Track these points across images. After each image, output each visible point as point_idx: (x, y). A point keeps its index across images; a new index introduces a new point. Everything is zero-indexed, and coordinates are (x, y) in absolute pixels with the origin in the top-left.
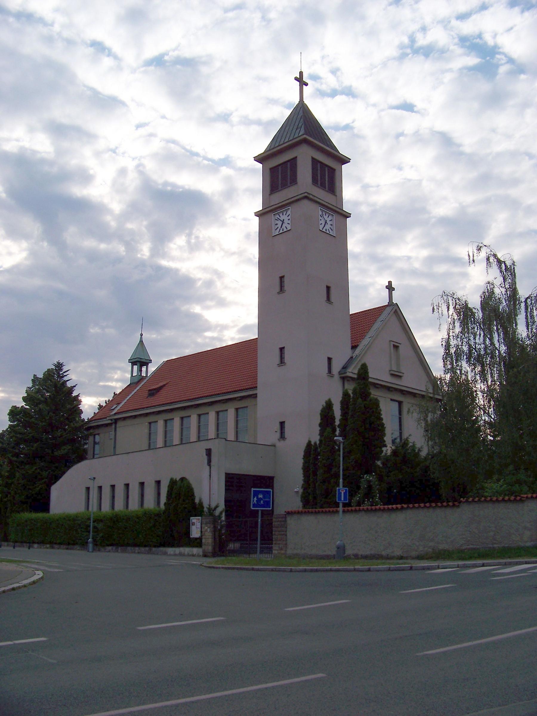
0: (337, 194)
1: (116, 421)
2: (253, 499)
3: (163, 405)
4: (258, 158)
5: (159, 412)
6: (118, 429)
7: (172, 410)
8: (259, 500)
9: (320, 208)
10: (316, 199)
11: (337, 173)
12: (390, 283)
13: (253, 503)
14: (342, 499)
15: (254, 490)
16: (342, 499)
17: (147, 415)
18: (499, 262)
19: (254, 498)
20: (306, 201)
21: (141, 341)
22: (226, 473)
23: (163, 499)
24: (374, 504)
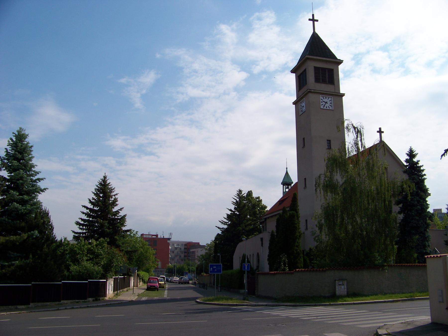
1: (266, 219)
2: (210, 268)
8: (214, 269)
12: (380, 129)
14: (246, 269)
16: (246, 269)
18: (355, 128)
19: (210, 268)
20: (310, 95)
21: (287, 173)
24: (413, 262)
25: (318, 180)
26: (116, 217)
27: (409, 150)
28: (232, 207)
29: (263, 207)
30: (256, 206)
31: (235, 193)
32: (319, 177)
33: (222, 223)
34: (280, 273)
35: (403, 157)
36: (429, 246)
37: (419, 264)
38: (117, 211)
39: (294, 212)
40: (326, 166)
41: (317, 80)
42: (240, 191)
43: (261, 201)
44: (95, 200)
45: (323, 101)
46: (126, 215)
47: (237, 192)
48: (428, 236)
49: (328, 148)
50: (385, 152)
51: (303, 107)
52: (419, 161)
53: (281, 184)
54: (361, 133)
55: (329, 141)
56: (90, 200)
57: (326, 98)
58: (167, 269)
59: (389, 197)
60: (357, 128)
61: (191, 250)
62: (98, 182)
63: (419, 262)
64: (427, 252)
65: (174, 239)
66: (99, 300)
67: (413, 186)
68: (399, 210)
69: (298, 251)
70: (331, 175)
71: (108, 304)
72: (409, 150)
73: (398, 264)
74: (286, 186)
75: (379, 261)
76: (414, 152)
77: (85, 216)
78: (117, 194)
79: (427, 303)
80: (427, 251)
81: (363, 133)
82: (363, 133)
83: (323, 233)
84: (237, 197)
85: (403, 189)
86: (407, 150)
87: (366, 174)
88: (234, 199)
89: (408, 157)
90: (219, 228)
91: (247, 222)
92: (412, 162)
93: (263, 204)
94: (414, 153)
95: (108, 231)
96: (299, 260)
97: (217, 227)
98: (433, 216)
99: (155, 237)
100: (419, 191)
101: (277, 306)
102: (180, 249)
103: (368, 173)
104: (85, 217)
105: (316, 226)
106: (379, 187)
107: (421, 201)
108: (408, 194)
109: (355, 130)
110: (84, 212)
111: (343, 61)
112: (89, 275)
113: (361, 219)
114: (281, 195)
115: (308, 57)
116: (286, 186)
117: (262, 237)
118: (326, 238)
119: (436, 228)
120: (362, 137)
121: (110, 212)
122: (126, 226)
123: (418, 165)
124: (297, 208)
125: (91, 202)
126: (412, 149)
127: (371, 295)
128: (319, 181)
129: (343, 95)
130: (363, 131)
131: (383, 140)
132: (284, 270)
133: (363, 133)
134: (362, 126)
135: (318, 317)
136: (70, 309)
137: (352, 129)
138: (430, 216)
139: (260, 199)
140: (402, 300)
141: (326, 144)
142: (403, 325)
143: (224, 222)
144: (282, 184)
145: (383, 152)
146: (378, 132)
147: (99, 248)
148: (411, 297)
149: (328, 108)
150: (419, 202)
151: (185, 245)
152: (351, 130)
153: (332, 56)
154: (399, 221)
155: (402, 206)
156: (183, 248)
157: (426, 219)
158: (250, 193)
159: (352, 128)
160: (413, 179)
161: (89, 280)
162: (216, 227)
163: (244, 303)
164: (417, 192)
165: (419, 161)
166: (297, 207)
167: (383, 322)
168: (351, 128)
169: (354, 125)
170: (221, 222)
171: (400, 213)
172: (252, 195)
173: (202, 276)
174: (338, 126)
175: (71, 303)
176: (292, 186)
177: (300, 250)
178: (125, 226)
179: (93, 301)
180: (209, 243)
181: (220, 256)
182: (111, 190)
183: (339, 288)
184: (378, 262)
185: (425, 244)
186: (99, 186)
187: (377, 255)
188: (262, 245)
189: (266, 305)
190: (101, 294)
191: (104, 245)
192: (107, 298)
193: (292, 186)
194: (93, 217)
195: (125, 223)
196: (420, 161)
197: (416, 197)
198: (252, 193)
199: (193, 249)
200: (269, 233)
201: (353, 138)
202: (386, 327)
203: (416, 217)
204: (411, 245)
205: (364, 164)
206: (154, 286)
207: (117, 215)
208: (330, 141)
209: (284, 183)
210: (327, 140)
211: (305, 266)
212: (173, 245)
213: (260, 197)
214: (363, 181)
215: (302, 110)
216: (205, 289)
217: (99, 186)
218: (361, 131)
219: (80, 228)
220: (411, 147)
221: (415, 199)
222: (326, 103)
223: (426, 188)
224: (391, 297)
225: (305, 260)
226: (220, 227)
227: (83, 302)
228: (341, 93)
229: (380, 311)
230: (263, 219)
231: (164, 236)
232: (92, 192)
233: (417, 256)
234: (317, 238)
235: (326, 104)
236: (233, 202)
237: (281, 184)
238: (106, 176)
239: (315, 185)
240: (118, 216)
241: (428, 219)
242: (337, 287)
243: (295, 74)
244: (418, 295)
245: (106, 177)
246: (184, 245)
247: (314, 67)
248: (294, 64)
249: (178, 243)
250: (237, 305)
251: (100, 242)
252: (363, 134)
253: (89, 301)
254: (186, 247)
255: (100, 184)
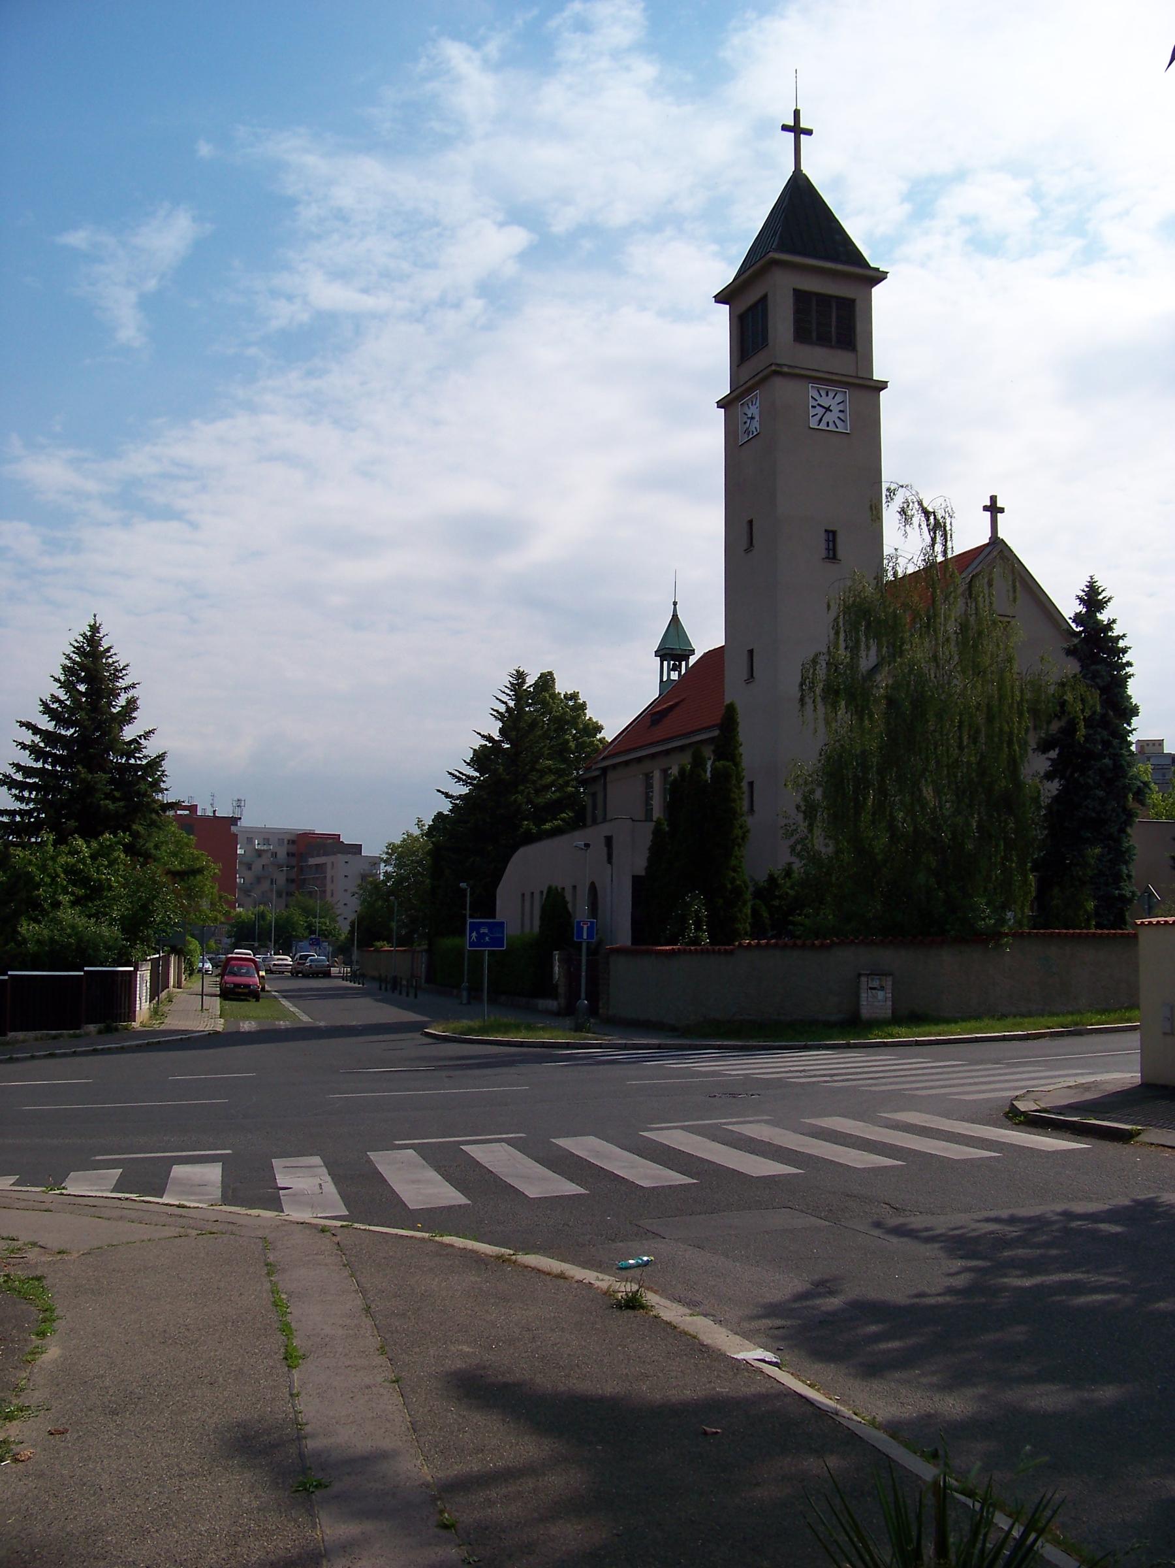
0: (859, 347)
1: (605, 770)
2: (470, 934)
3: (652, 744)
4: (718, 297)
5: (653, 756)
6: (609, 786)
7: (667, 753)
8: (481, 936)
9: (811, 385)
10: (797, 371)
11: (859, 306)
12: (993, 499)
13: (470, 939)
14: (585, 937)
15: (470, 922)
16: (585, 937)
17: (639, 760)
18: (927, 513)
20: (778, 382)
21: (675, 617)
22: (633, 876)
23: (537, 923)
24: (1083, 925)
25: (811, 671)
26: (130, 762)
27: (1087, 586)
28: (494, 729)
29: (591, 727)
30: (567, 724)
31: (505, 680)
32: (814, 662)
33: (458, 778)
34: (714, 951)
35: (1069, 607)
36: (1129, 876)
37: (1099, 931)
38: (134, 741)
39: (728, 764)
40: (833, 629)
41: (802, 335)
42: (520, 676)
43: (583, 707)
44: (61, 702)
45: (819, 405)
46: (165, 753)
47: (511, 679)
48: (1129, 847)
49: (827, 558)
50: (1015, 591)
51: (752, 418)
52: (1114, 621)
53: (656, 656)
54: (945, 529)
55: (831, 535)
56: (44, 704)
57: (827, 395)
58: (233, 926)
59: (1023, 733)
60: (934, 513)
61: (312, 861)
62: (71, 644)
63: (1098, 926)
64: (1124, 896)
65: (249, 820)
66: (117, 1029)
67: (1095, 699)
68: (1048, 769)
69: (738, 882)
70: (852, 659)
71: (153, 1042)
72: (1087, 586)
73: (1042, 931)
74: (672, 662)
75: (987, 920)
76: (1100, 594)
77: (30, 755)
78: (133, 686)
79: (1134, 1038)
80: (1124, 892)
81: (951, 530)
82: (949, 532)
83: (817, 832)
84: (510, 696)
85: (1063, 704)
86: (1079, 587)
87: (956, 658)
88: (500, 700)
89: (1081, 609)
90: (447, 795)
91: (541, 777)
92: (1095, 625)
93: (587, 718)
94: (1100, 597)
95: (111, 807)
96: (740, 911)
97: (443, 793)
98: (1147, 790)
99: (187, 812)
100: (1109, 711)
101: (691, 1048)
102: (275, 855)
103: (961, 653)
104: (26, 759)
105: (797, 809)
106: (995, 703)
107: (1116, 742)
108: (1078, 723)
109: (928, 520)
110: (25, 744)
111: (887, 273)
112: (82, 953)
113: (938, 792)
114: (650, 693)
115: (777, 256)
116: (672, 662)
117: (609, 834)
118: (827, 845)
119: (1148, 817)
120: (949, 543)
121: (114, 743)
122: (166, 790)
123: (1110, 634)
124: (737, 752)
125: (47, 710)
126: (1095, 582)
127: (964, 1020)
128: (814, 674)
129: (883, 385)
130: (951, 524)
131: (1001, 535)
132: (696, 941)
133: (949, 532)
134: (949, 509)
135: (836, 1078)
136: (45, 1056)
137: (918, 518)
138: (1139, 788)
139: (581, 701)
140: (1052, 1035)
141: (823, 545)
142: (1073, 1091)
143: (464, 777)
144: (657, 654)
145: (1008, 591)
146: (986, 508)
147: (103, 865)
148: (1077, 1024)
149: (832, 428)
150: (1107, 744)
151: (292, 842)
152: (915, 521)
153: (853, 256)
154: (1046, 800)
155: (1058, 755)
156: (282, 852)
157: (1126, 797)
158: (546, 681)
159: (920, 512)
160: (1095, 676)
161: (86, 969)
162: (439, 791)
163: (585, 1039)
164: (1104, 716)
165: (1114, 621)
166: (736, 748)
167: (1022, 1088)
168: (916, 513)
169: (925, 505)
170: (453, 775)
171: (1049, 776)
172: (553, 687)
173: (378, 951)
174: (874, 505)
175: (36, 1039)
176: (690, 666)
177: (744, 882)
178: (162, 791)
179: (100, 1032)
180: (398, 842)
181: (469, 890)
182: (116, 670)
183: (870, 999)
184: (986, 923)
185: (1120, 870)
186: (74, 656)
187: (981, 901)
188: (610, 859)
189: (659, 1047)
190: (123, 1011)
191: (116, 854)
192: (136, 1025)
193: (690, 666)
194: (57, 760)
195: (164, 782)
196: (1117, 622)
197: (1099, 729)
198: (553, 680)
199: (318, 855)
200: (633, 821)
201: (924, 545)
202: (1032, 1096)
203: (1097, 792)
204: (1080, 873)
205: (952, 627)
206: (247, 986)
207: (137, 755)
208: (834, 533)
209: (664, 653)
210: (826, 531)
211: (758, 931)
212: (250, 840)
213: (578, 693)
214: (945, 677)
215: (748, 429)
216: (400, 993)
217: (74, 656)
218: (945, 523)
219: (17, 798)
220: (1091, 577)
221: (1098, 737)
222: (828, 409)
223: (1131, 703)
224: (1019, 1026)
225: (755, 912)
226: (450, 793)
227: (71, 1036)
228: (874, 378)
229: (997, 1062)
230: (597, 769)
231: (215, 811)
232: (52, 676)
233: (1095, 906)
234: (799, 847)
235: (828, 413)
236: (495, 710)
237: (656, 656)
238: (98, 625)
239: (801, 685)
240: (140, 758)
241: (1130, 796)
242: (863, 995)
243: (727, 307)
244: (1093, 1021)
245: (98, 628)
246: (286, 842)
247: (794, 289)
248: (726, 274)
249: (267, 836)
250: (568, 1046)
251: (100, 844)
252: (951, 535)
253: (87, 1034)
254: (293, 849)
255: (79, 650)
